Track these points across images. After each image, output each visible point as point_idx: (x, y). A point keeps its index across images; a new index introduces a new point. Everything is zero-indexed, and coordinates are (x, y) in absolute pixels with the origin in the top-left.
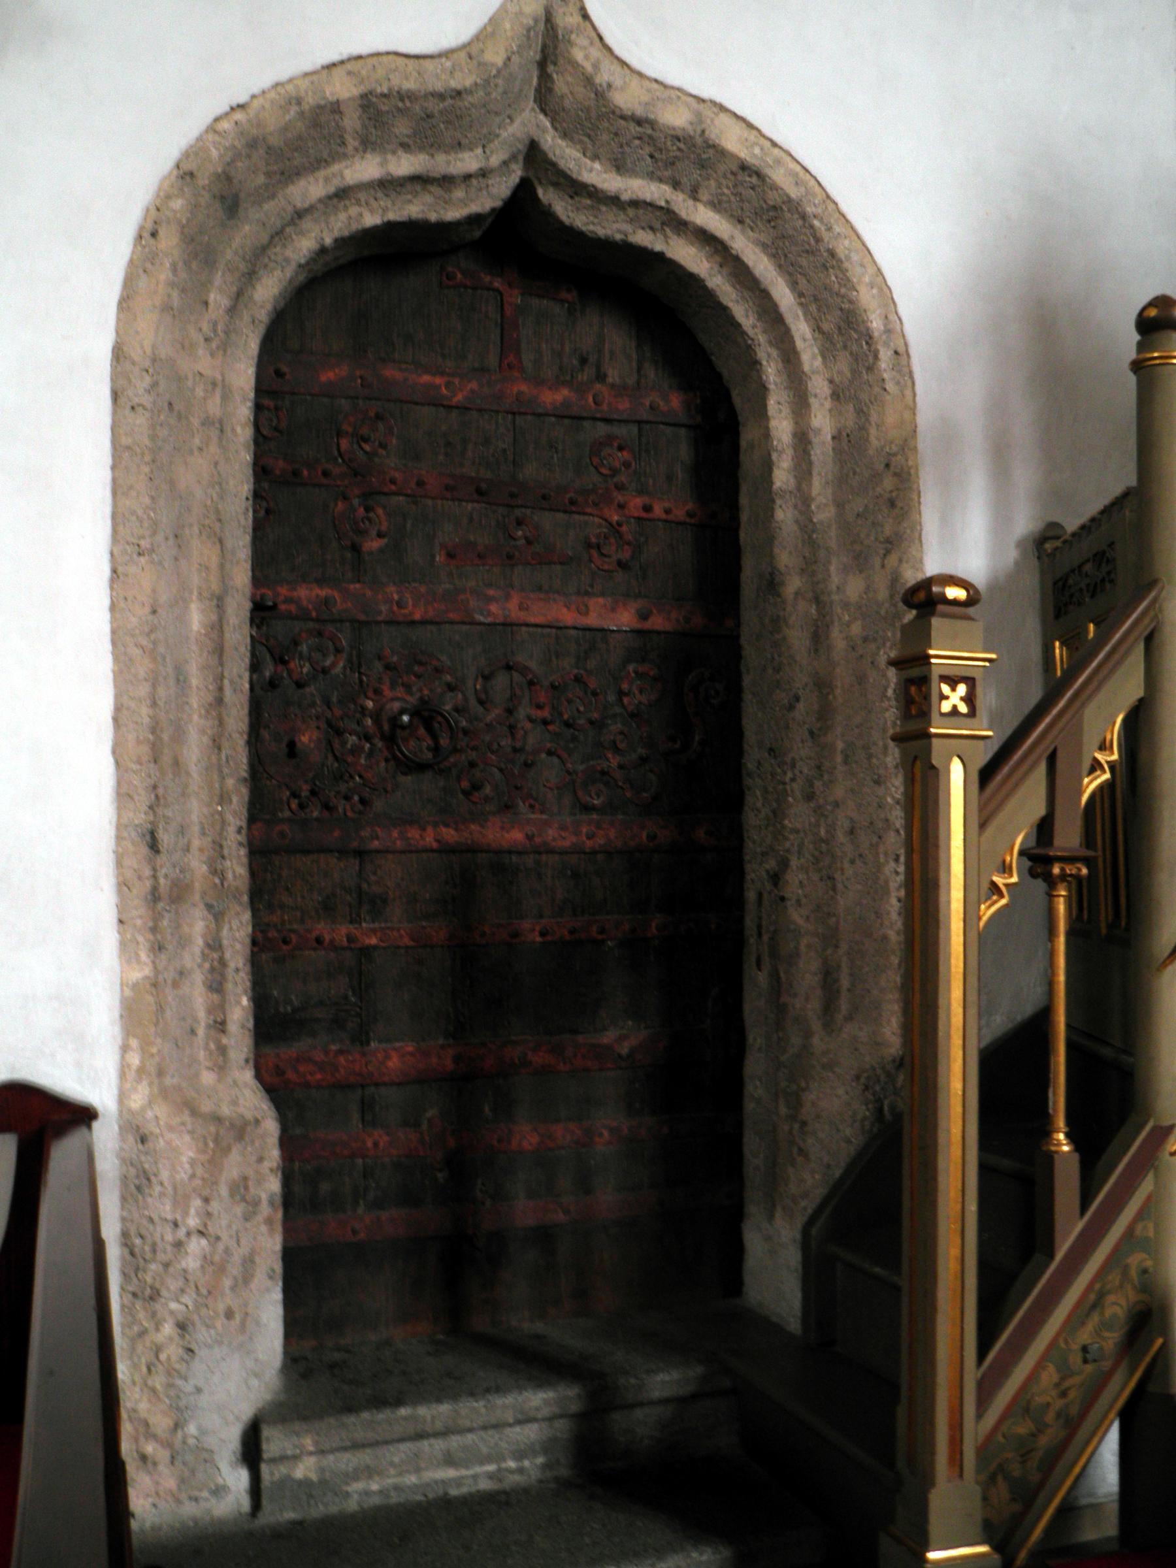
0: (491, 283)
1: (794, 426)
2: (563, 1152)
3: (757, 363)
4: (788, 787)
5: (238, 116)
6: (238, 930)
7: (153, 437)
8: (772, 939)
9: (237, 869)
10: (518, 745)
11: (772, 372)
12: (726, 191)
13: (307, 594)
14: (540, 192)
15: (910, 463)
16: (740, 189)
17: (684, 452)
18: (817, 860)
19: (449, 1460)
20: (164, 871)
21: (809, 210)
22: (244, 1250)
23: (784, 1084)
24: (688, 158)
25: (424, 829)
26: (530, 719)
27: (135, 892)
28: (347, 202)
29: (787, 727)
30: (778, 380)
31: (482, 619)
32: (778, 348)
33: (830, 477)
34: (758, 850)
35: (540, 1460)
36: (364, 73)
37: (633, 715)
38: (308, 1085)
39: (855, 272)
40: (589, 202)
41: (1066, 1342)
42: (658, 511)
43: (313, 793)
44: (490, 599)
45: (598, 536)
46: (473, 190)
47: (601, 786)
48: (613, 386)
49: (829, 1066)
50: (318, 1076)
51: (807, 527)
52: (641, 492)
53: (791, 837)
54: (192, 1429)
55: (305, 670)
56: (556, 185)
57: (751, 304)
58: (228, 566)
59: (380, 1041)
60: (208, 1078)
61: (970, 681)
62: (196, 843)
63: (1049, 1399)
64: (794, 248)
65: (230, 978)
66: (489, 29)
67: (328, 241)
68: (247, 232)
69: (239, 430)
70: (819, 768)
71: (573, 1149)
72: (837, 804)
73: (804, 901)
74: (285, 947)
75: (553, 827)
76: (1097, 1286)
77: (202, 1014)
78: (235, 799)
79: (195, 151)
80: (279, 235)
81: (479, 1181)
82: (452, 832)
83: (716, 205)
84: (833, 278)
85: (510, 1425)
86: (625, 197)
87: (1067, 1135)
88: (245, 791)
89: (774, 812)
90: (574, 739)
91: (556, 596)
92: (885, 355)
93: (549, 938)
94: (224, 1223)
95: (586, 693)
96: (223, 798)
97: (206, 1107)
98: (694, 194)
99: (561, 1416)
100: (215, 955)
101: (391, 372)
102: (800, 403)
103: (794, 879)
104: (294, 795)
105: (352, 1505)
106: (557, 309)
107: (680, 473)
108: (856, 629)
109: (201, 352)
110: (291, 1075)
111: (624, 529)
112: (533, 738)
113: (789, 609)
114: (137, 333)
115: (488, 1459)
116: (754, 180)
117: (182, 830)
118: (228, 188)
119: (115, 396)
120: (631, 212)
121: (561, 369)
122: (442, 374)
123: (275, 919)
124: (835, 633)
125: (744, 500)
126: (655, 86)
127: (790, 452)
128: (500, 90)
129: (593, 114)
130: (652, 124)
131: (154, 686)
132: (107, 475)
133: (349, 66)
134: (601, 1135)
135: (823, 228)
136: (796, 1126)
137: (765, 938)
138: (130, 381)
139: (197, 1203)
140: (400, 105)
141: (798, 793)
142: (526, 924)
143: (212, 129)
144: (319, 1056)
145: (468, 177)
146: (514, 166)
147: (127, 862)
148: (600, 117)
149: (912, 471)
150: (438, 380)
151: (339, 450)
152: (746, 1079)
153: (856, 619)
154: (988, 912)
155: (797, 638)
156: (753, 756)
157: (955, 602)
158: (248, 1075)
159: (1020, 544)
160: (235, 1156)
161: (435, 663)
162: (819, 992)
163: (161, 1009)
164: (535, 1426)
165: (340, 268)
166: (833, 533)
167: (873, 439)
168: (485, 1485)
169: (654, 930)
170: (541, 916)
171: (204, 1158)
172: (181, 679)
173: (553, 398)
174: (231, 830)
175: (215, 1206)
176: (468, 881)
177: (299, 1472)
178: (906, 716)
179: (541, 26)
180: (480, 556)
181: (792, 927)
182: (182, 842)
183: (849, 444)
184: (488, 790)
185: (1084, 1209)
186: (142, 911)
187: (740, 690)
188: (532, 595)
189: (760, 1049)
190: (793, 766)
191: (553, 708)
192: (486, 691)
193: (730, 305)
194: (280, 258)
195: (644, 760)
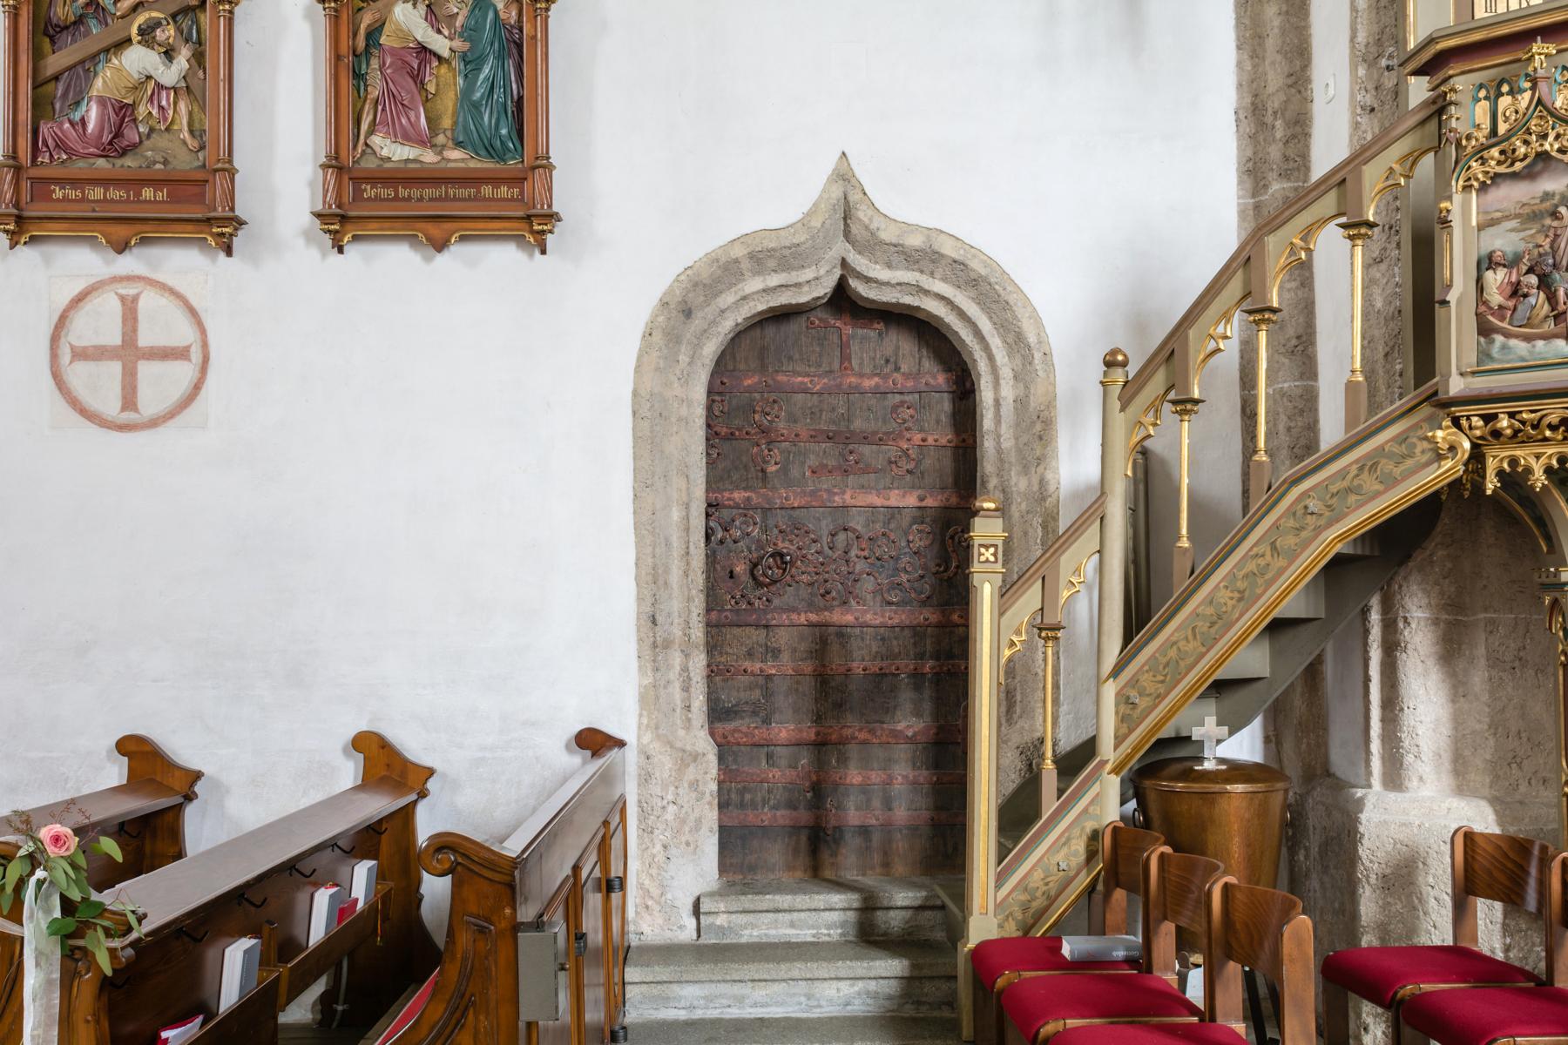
1: (996, 396)
6: (699, 663)
9: (698, 633)
11: (982, 366)
13: (738, 496)
19: (792, 925)
21: (993, 280)
22: (697, 814)
38: (738, 744)
39: (1019, 311)
42: (930, 441)
51: (999, 451)
52: (921, 430)
54: (669, 896)
60: (681, 733)
61: (996, 546)
68: (697, 323)
71: (881, 785)
75: (873, 615)
79: (670, 291)
80: (714, 323)
83: (944, 279)
92: (1038, 356)
96: (689, 599)
97: (679, 745)
98: (932, 274)
101: (781, 378)
105: (744, 940)
106: (872, 334)
108: (1024, 506)
110: (730, 739)
112: (860, 566)
115: (813, 927)
117: (669, 615)
118: (681, 309)
119: (634, 413)
124: (1014, 508)
139: (672, 788)
142: (855, 664)
143: (676, 280)
144: (744, 729)
154: (1007, 653)
160: (692, 768)
163: (657, 698)
172: (668, 544)
173: (868, 383)
175: (680, 791)
176: (824, 641)
177: (718, 922)
183: (1021, 403)
195: (922, 577)
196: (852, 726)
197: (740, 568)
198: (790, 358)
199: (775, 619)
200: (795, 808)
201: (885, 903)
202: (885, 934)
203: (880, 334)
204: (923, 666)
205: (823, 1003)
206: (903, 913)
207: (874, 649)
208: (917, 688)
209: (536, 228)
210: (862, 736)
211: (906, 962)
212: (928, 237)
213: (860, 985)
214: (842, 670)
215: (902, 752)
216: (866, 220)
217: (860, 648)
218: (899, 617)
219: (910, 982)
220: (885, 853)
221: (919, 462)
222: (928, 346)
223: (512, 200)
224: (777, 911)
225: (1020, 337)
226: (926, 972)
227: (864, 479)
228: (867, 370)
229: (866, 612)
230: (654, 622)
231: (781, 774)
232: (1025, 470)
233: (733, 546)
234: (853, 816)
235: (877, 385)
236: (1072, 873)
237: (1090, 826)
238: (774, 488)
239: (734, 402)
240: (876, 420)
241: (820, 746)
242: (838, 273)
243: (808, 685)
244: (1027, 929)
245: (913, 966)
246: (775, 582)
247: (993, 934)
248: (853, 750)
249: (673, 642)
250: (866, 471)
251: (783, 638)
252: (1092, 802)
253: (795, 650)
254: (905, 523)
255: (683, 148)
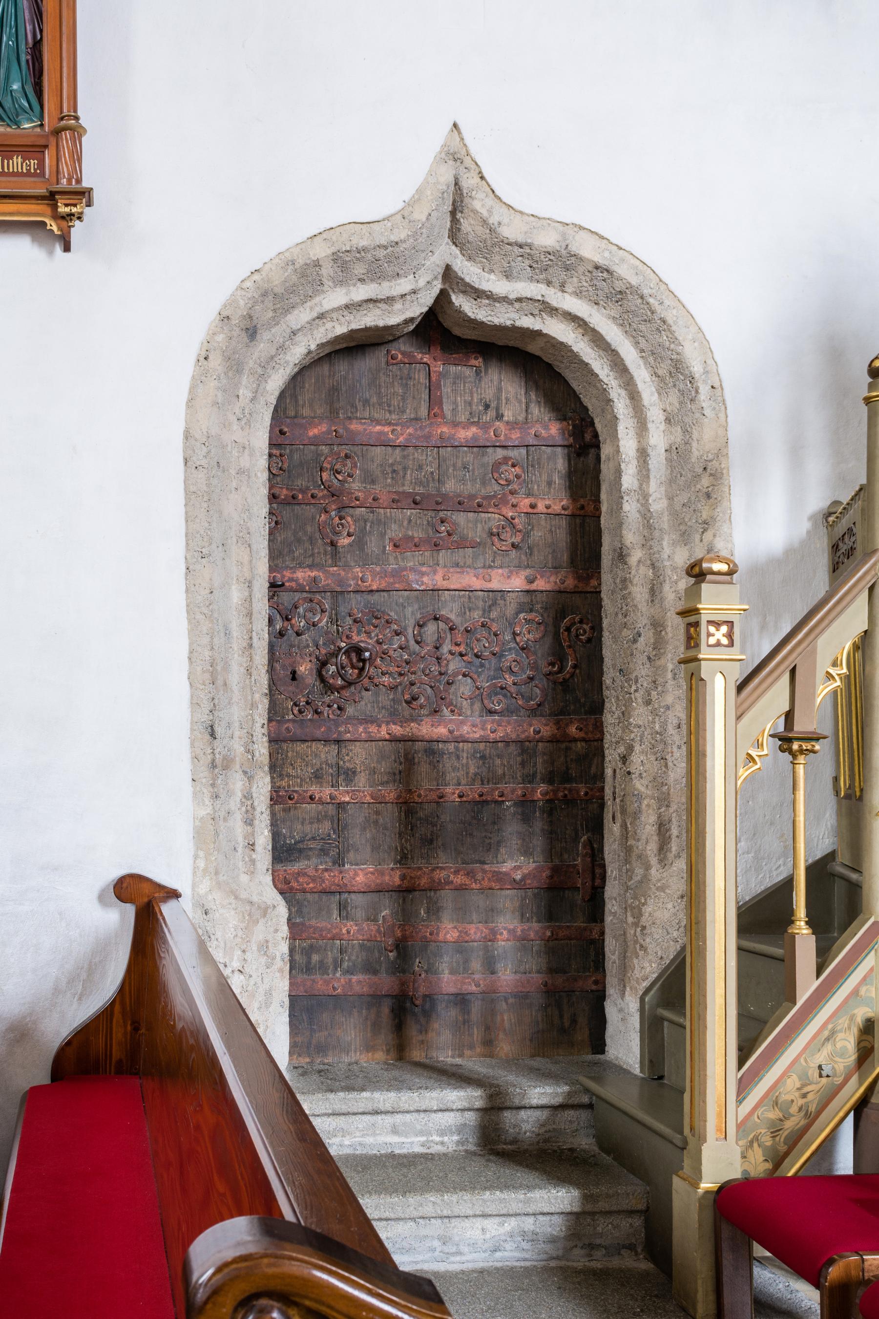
0: (422, 359)
1: (638, 448)
2: (475, 944)
3: (609, 401)
4: (633, 696)
5: (256, 277)
7: (208, 485)
8: (622, 801)
9: (262, 749)
10: (443, 670)
11: (621, 406)
12: (585, 284)
13: (302, 575)
14: (453, 298)
15: (723, 466)
16: (595, 282)
17: (561, 464)
18: (654, 747)
19: (395, 1131)
20: (218, 750)
21: (646, 292)
23: (630, 901)
24: (557, 265)
25: (380, 726)
26: (451, 653)
27: (201, 762)
28: (325, 320)
29: (632, 655)
30: (626, 412)
31: (418, 587)
32: (626, 390)
33: (663, 478)
34: (613, 740)
35: (455, 1138)
36: (334, 238)
37: (523, 649)
38: (304, 891)
39: (680, 333)
40: (487, 301)
41: (806, 1061)
42: (541, 507)
43: (308, 703)
44: (423, 574)
45: (498, 527)
46: (408, 302)
47: (501, 697)
48: (508, 423)
49: (662, 889)
50: (311, 885)
51: (646, 514)
52: (529, 494)
53: (635, 730)
55: (302, 624)
56: (464, 292)
57: (605, 360)
58: (254, 561)
59: (352, 864)
60: (244, 878)
61: (730, 624)
62: (237, 733)
63: (793, 1098)
64: (636, 319)
65: (257, 817)
66: (416, 197)
67: (313, 347)
68: (262, 348)
69: (259, 474)
70: (654, 682)
72: (668, 708)
73: (644, 775)
74: (290, 802)
76: (830, 1026)
77: (240, 839)
78: (260, 706)
79: (231, 303)
80: (282, 348)
81: (418, 960)
82: (399, 728)
83: (578, 294)
84: (665, 338)
85: (435, 1111)
86: (512, 296)
87: (807, 923)
88: (266, 701)
89: (623, 713)
90: (482, 665)
91: (468, 569)
93: (464, 799)
94: (254, 967)
95: (490, 634)
96: (253, 706)
97: (243, 895)
98: (562, 287)
99: (469, 1110)
100: (249, 803)
101: (354, 426)
102: (642, 426)
103: (637, 759)
104: (295, 704)
106: (467, 371)
107: (556, 479)
109: (235, 427)
110: (294, 884)
111: (516, 520)
112: (454, 665)
113: (633, 572)
114: (198, 421)
115: (421, 1133)
116: (605, 275)
117: (229, 725)
120: (517, 305)
121: (471, 414)
122: (390, 424)
123: (284, 783)
124: (667, 588)
125: (603, 496)
126: (532, 218)
127: (635, 462)
128: (424, 236)
129: (489, 243)
130: (530, 246)
131: (212, 638)
132: (182, 510)
133: (324, 236)
134: (501, 934)
135: (657, 303)
136: (639, 929)
137: (618, 800)
138: (194, 451)
140: (358, 255)
141: (640, 700)
144: (311, 872)
145: (403, 296)
146: (435, 283)
147: (197, 744)
148: (494, 245)
149: (724, 471)
150: (387, 429)
151: (321, 480)
152: (606, 900)
153: (682, 578)
154: (743, 773)
155: (639, 592)
156: (609, 675)
157: (719, 573)
158: (269, 879)
159: (811, 518)
160: (261, 926)
161: (387, 617)
162: (655, 838)
163: (217, 834)
164: (452, 1114)
165: (320, 359)
166: (666, 518)
167: (694, 450)
168: (418, 1149)
169: (539, 796)
170: (459, 784)
171: (243, 925)
172: (227, 633)
173: (464, 434)
174: (258, 725)
176: (409, 760)
178: (688, 647)
179: (452, 188)
180: (416, 546)
181: (636, 793)
182: (229, 732)
183: (677, 454)
184: (422, 700)
185: (819, 974)
186: (206, 774)
187: (601, 630)
188: (451, 570)
189: (615, 878)
190: (637, 682)
191: (467, 645)
192: (420, 634)
193: (590, 362)
194: (282, 361)
195: (531, 679)
196: (446, 868)
197: (305, 668)
198: (366, 402)
199: (348, 731)
200: (375, 972)
201: (517, 1102)
202: (515, 1141)
203: (478, 373)
204: (534, 790)
205: (465, 1249)
206: (538, 1113)
207: (472, 770)
208: (526, 819)
209: (63, 209)
210: (458, 880)
211: (575, 1193)
212: (564, 235)
213: (511, 1224)
214: (433, 796)
215: (508, 899)
216: (485, 214)
217: (455, 769)
218: (506, 729)
219: (579, 1225)
220: (488, 1028)
221: (527, 535)
222: (537, 388)
223: (28, 174)
224: (377, 1112)
225: (678, 367)
226: (603, 1205)
227: (459, 555)
228: (463, 418)
229: (462, 723)
230: (213, 735)
231: (358, 928)
232: (685, 538)
233: (296, 640)
234: (447, 980)
235: (475, 438)
236: (839, 1080)
237: (862, 1013)
238: (347, 566)
239: (296, 456)
240: (473, 480)
241: (406, 892)
242: (438, 286)
243: (390, 815)
244: (778, 1160)
245: (587, 1198)
246: (350, 684)
247: (735, 1173)
248: (447, 897)
249: (232, 760)
250: (462, 544)
251: (358, 755)
252: (864, 980)
253: (373, 772)
254: (510, 611)
255: (241, 132)
